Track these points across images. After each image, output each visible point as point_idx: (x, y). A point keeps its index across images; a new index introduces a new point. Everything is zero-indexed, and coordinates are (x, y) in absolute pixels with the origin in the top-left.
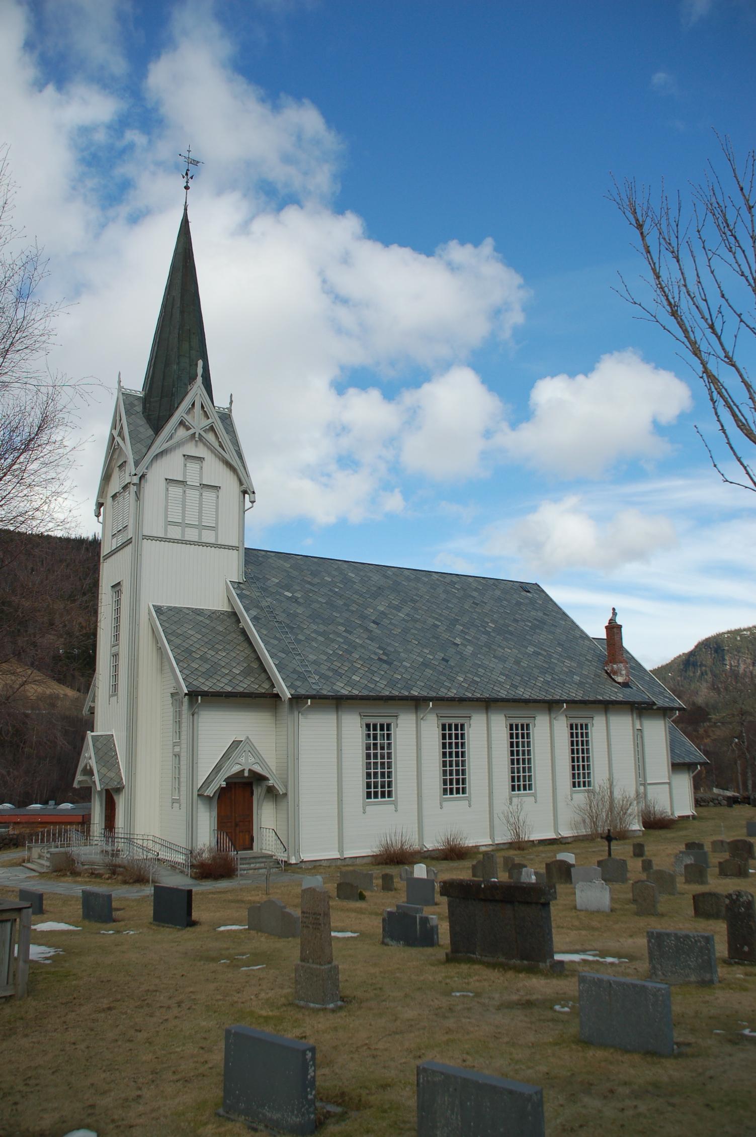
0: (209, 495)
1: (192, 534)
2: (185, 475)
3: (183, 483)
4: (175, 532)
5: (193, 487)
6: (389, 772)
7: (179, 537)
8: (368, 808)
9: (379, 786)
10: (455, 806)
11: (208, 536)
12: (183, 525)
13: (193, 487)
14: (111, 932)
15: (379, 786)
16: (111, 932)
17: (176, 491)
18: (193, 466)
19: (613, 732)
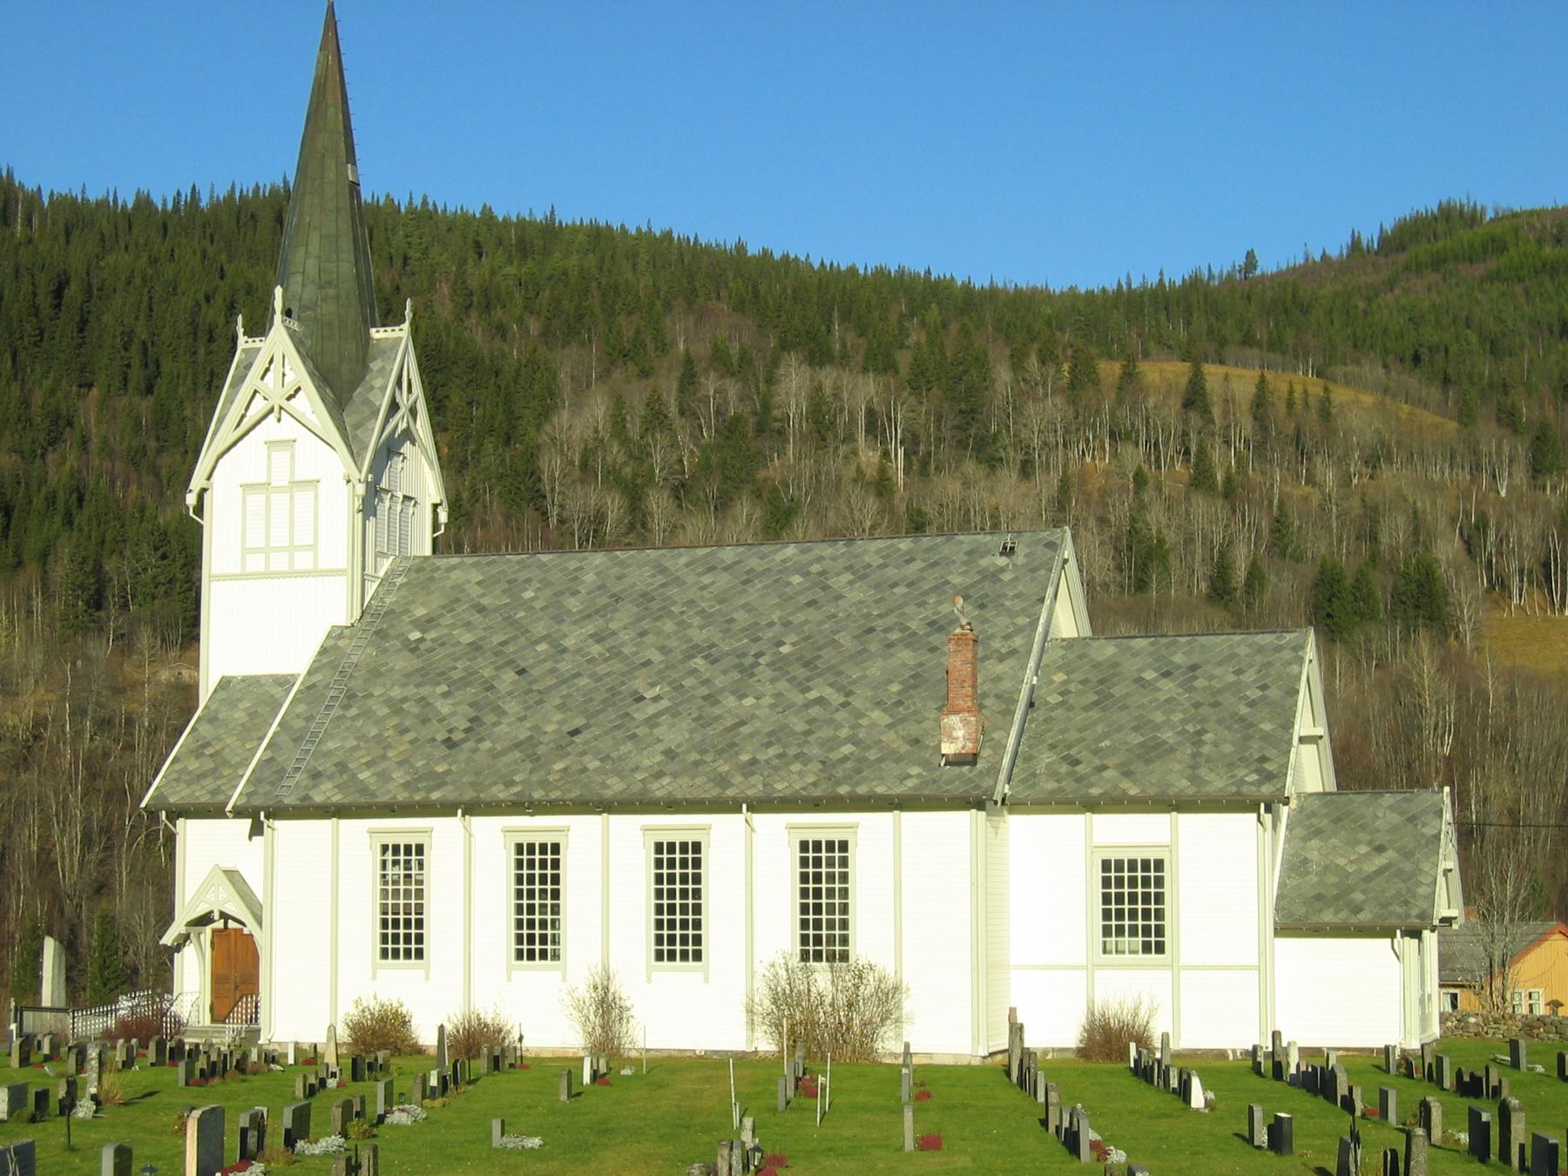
0: (304, 498)
1: (279, 562)
2: (269, 476)
3: (265, 486)
4: (255, 563)
5: (279, 490)
6: (553, 921)
7: (285, 568)
8: (379, 972)
9: (402, 935)
10: (403, 970)
11: (303, 561)
12: (267, 550)
13: (279, 490)
14: (535, 1142)
15: (402, 935)
16: (535, 1142)
17: (257, 500)
18: (282, 457)
19: (341, 830)
